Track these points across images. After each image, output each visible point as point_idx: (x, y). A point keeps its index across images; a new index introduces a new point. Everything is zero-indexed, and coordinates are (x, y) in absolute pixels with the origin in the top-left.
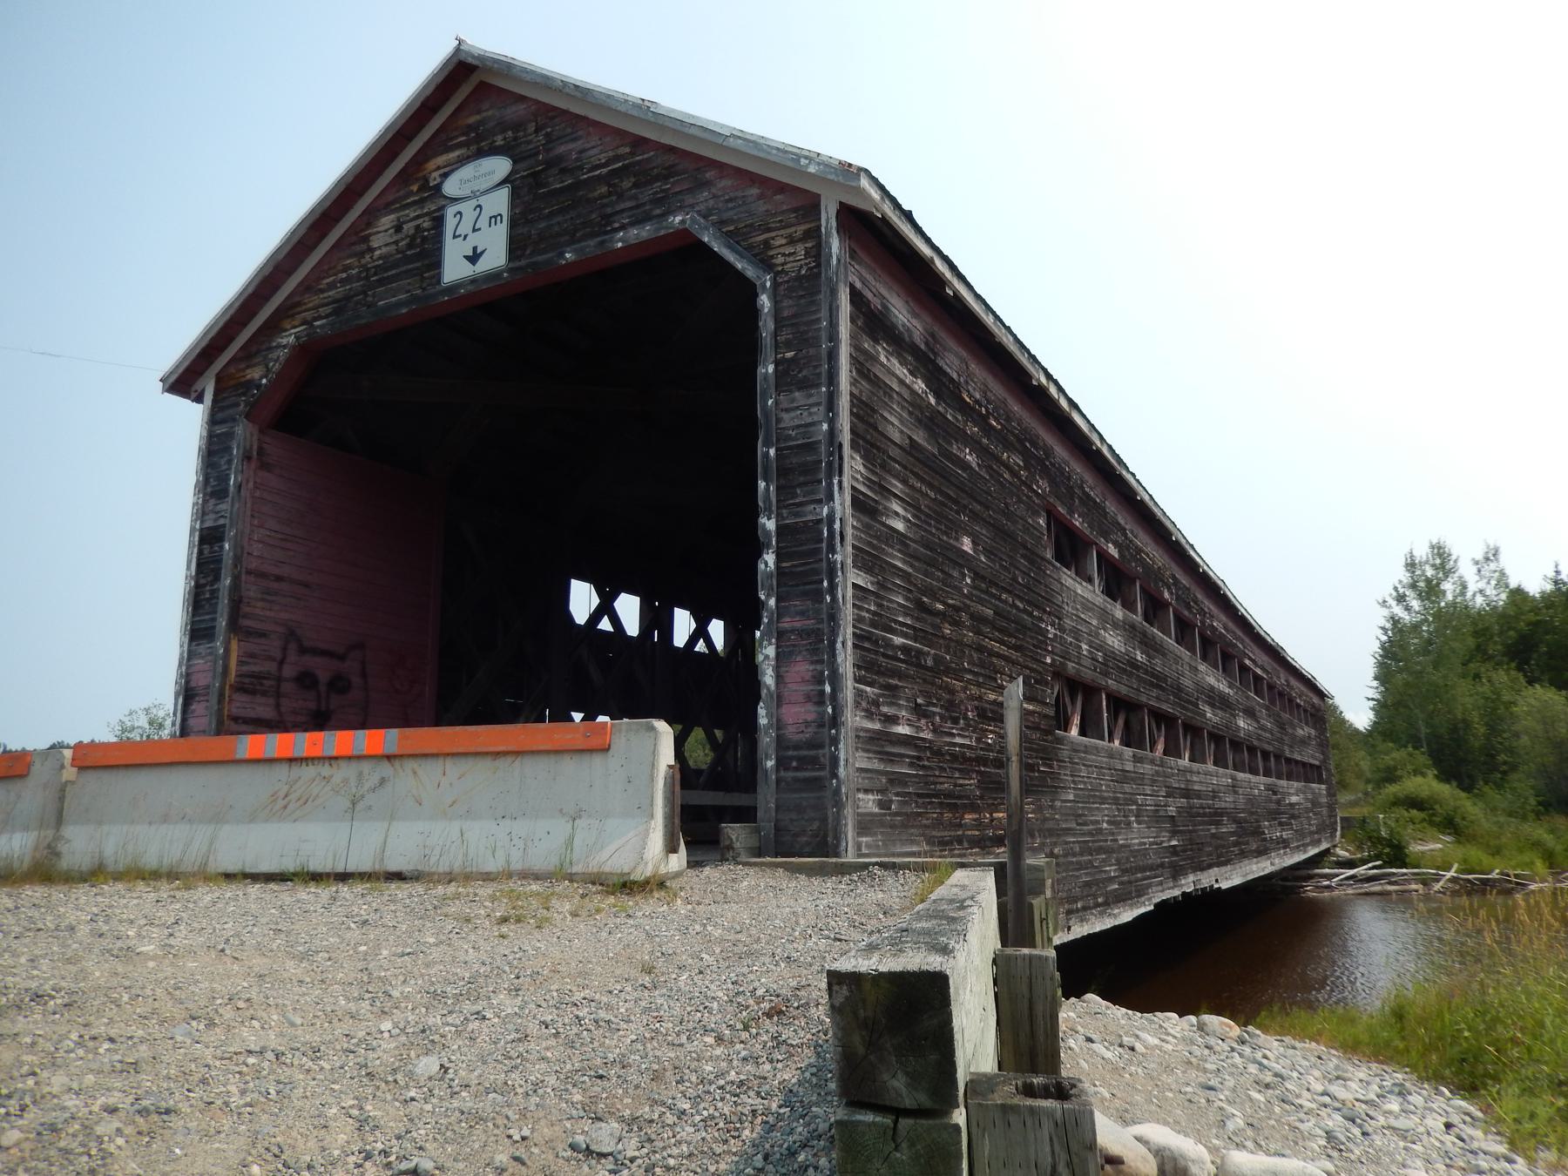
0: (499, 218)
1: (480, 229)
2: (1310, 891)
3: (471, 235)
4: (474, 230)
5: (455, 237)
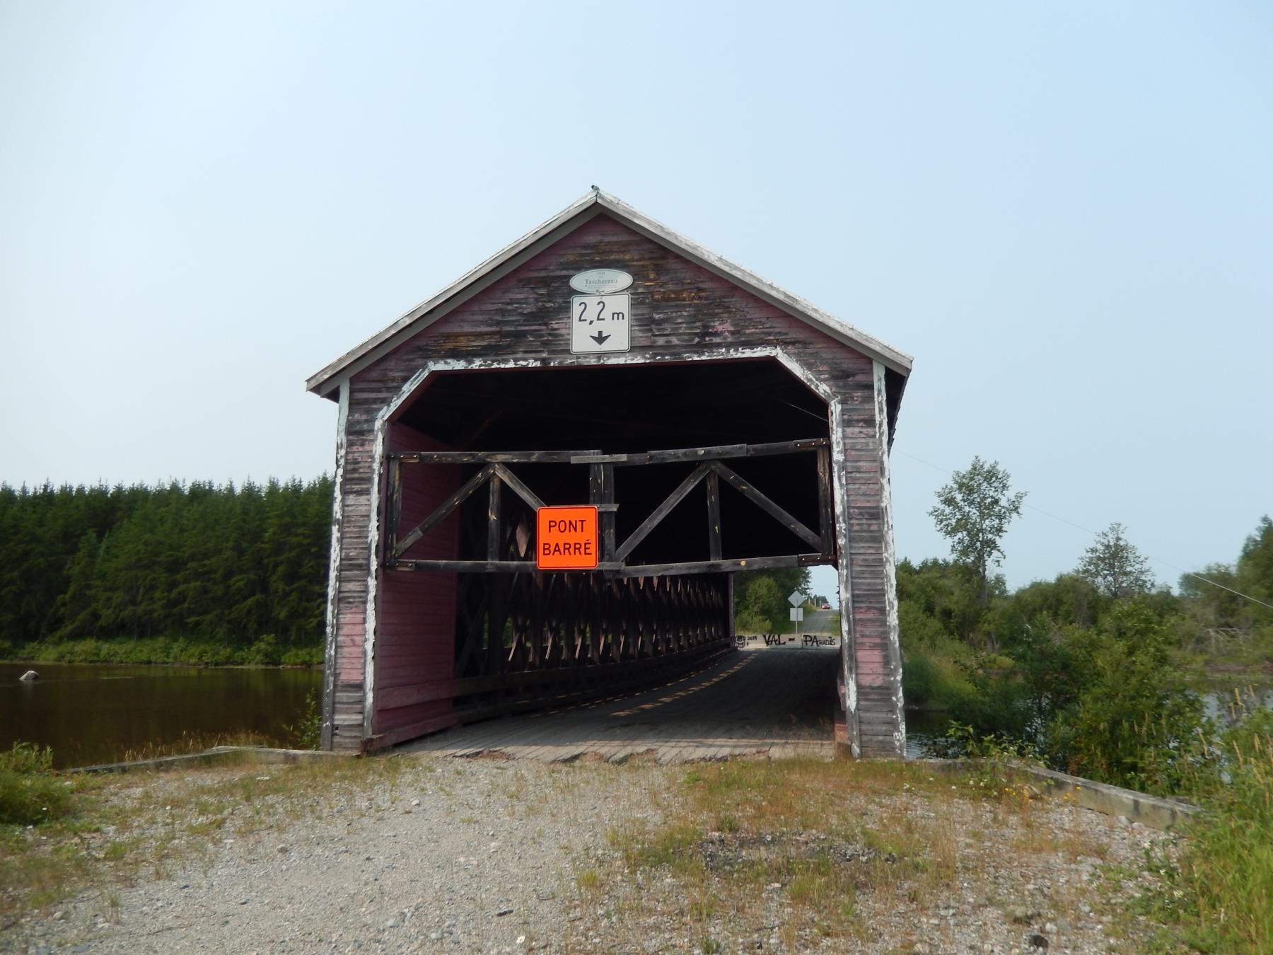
0: (621, 315)
1: (604, 319)
3: (596, 323)
4: (598, 319)
5: (580, 320)
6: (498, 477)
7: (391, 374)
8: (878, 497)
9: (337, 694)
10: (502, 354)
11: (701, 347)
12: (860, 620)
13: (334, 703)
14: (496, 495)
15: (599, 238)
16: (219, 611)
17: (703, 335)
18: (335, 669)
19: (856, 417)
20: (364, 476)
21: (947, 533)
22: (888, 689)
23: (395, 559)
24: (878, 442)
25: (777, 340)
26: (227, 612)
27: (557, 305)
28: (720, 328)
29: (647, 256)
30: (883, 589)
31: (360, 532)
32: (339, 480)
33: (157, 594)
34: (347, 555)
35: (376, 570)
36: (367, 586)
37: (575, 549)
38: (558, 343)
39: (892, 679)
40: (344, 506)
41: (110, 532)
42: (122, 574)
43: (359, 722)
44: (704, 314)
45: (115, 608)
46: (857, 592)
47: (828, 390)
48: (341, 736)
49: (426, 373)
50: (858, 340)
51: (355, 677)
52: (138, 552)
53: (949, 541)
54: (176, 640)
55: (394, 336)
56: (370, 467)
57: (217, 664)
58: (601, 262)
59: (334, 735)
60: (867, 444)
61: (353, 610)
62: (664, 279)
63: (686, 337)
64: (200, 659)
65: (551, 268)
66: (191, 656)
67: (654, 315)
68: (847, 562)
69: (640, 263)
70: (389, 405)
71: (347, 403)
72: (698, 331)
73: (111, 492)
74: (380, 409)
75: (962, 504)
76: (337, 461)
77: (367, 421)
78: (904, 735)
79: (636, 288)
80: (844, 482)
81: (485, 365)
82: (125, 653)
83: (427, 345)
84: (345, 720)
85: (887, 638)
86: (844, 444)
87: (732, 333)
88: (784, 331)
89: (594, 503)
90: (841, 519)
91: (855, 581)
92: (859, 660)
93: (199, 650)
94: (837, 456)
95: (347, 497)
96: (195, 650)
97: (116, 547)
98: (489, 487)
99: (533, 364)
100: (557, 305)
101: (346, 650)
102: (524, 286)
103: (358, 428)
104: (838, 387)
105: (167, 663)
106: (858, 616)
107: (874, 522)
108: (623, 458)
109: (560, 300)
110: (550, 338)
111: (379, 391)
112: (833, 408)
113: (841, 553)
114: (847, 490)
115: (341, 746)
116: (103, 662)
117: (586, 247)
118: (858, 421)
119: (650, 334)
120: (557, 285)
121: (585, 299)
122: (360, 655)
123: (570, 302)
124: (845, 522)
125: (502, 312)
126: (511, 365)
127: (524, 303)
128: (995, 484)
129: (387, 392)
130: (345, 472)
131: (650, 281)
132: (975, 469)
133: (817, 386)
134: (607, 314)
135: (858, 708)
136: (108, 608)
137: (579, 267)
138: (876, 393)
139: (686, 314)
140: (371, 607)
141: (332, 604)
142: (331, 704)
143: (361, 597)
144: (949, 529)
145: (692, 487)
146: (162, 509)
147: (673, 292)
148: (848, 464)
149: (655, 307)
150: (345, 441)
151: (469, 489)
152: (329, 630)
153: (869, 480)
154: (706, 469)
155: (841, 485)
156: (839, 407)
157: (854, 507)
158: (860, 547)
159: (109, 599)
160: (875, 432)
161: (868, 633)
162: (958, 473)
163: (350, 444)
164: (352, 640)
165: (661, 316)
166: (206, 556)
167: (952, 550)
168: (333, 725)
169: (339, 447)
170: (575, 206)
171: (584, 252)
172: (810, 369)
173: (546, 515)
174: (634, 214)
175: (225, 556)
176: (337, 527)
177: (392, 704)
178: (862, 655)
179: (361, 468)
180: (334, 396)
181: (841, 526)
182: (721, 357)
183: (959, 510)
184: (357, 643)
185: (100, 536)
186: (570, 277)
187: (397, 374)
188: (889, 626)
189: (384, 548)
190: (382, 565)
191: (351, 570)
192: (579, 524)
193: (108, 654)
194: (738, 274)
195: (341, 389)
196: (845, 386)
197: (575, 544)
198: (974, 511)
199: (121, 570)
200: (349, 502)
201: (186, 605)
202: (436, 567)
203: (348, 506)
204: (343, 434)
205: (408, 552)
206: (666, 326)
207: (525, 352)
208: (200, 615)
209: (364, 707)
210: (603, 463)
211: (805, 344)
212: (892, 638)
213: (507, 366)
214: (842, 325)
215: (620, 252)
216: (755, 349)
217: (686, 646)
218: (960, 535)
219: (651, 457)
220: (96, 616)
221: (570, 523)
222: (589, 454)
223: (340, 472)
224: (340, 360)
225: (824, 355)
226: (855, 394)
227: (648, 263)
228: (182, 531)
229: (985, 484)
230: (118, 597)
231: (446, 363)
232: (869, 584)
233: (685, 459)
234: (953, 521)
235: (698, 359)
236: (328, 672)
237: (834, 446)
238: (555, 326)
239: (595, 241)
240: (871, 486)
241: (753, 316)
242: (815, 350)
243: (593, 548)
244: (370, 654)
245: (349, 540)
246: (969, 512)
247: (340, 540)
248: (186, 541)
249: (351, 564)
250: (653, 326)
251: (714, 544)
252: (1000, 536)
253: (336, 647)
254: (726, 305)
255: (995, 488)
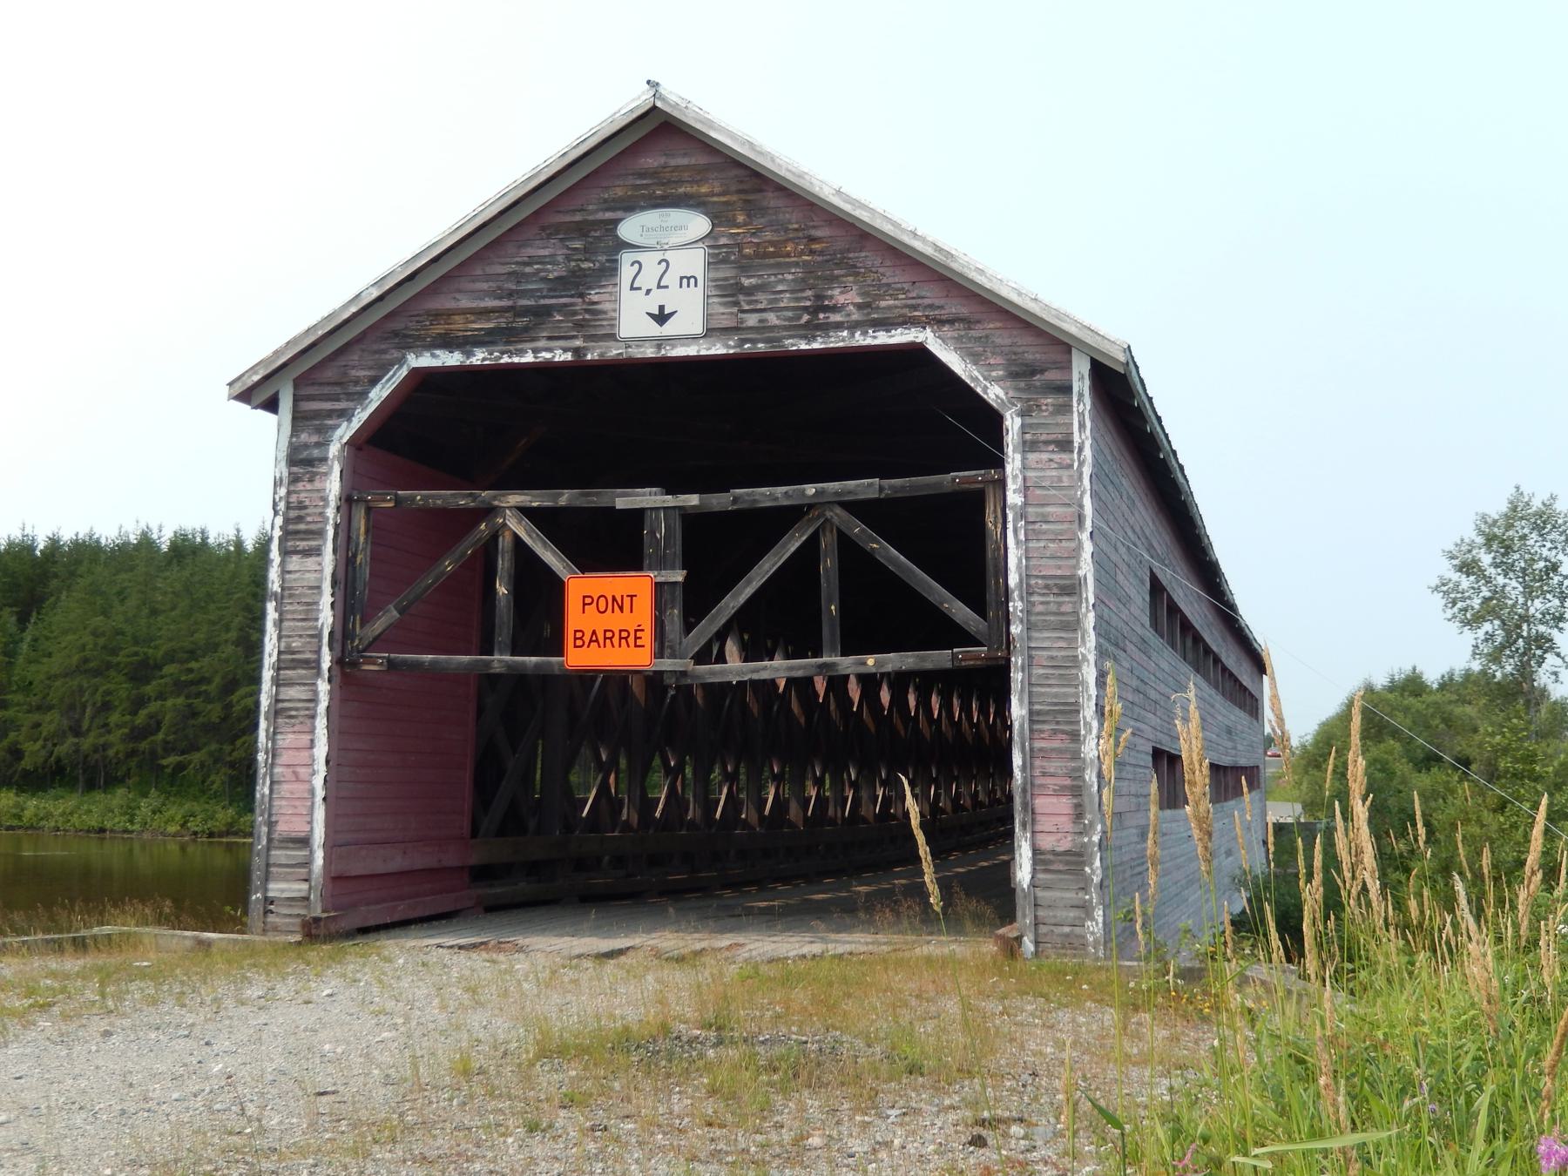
0: (692, 281)
1: (667, 287)
2: (775, 783)
3: (655, 292)
4: (659, 287)
5: (632, 288)
6: (510, 529)
7: (354, 373)
8: (1073, 562)
9: (273, 853)
10: (516, 342)
11: (811, 330)
12: (1041, 750)
13: (268, 865)
14: (507, 557)
15: (662, 160)
16: (214, 746)
17: (815, 311)
18: (270, 815)
19: (1044, 437)
20: (313, 527)
21: (1466, 623)
22: (1080, 854)
23: (359, 652)
24: (1076, 474)
25: (927, 317)
26: (227, 748)
27: (597, 264)
28: (841, 299)
29: (733, 188)
30: (1076, 703)
31: (307, 611)
32: (277, 533)
33: (114, 718)
34: (288, 646)
35: (330, 670)
36: (316, 693)
37: (621, 638)
38: (594, 323)
39: (1086, 840)
40: (284, 572)
41: (38, 613)
42: (58, 683)
43: (303, 894)
44: (818, 278)
45: (46, 740)
46: (1037, 707)
47: (1001, 394)
48: (278, 914)
49: (404, 372)
50: (1044, 316)
51: (299, 828)
52: (83, 647)
53: (1469, 638)
54: (145, 795)
55: (355, 315)
56: (322, 514)
57: (211, 835)
58: (663, 197)
59: (267, 912)
60: (1060, 479)
61: (296, 729)
62: (759, 222)
63: (790, 314)
64: (182, 826)
65: (590, 207)
66: (171, 820)
67: (743, 280)
68: (1023, 660)
69: (723, 199)
70: (349, 420)
71: (289, 417)
72: (808, 303)
73: (41, 546)
74: (337, 427)
75: (1491, 571)
76: (275, 504)
77: (318, 445)
78: (1101, 925)
79: (716, 239)
80: (1022, 537)
81: (490, 359)
82: (63, 814)
83: (406, 328)
84: (283, 891)
85: (1081, 778)
86: (1025, 479)
87: (859, 306)
88: (937, 302)
89: (650, 569)
90: (1016, 594)
91: (1035, 689)
92: (1038, 810)
93: (182, 812)
94: (1014, 498)
95: (288, 559)
96: (175, 811)
97: (47, 638)
98: (497, 545)
99: (562, 357)
100: (597, 264)
101: (285, 787)
102: (549, 237)
103: (304, 455)
104: (1018, 389)
105: (132, 832)
106: (1038, 744)
107: (1067, 599)
108: (693, 500)
109: (603, 258)
110: (587, 316)
111: (335, 398)
112: (1008, 423)
113: (1015, 647)
114: (1027, 550)
115: (276, 929)
116: (27, 828)
117: (642, 175)
118: (1047, 443)
119: (735, 310)
120: (598, 234)
121: (641, 257)
122: (306, 795)
123: (617, 261)
124: (1021, 599)
125: (516, 276)
126: (529, 358)
127: (549, 263)
128: (1554, 536)
129: (347, 401)
130: (287, 521)
131: (738, 227)
132: (1514, 509)
133: (985, 389)
134: (671, 279)
135: (1033, 885)
136: (35, 741)
137: (631, 206)
138: (1075, 399)
139: (790, 277)
140: (321, 723)
141: (266, 719)
142: (263, 867)
143: (307, 709)
144: (1469, 616)
145: (797, 544)
146: (124, 576)
147: (772, 243)
148: (1030, 509)
149: (744, 267)
150: (285, 474)
151: (467, 548)
152: (261, 757)
153: (1061, 534)
154: (819, 517)
155: (1018, 542)
156: (1018, 421)
157: (1037, 577)
158: (1043, 638)
159: (37, 725)
160: (1073, 460)
161: (1052, 770)
162: (1484, 518)
163: (294, 479)
164: (294, 772)
165: (753, 281)
166: (192, 654)
167: (1474, 653)
168: (266, 898)
169: (277, 483)
170: (622, 112)
171: (638, 182)
172: (976, 363)
173: (579, 586)
174: (711, 124)
175: (223, 655)
176: (274, 603)
177: (358, 868)
178: (1041, 803)
179: (308, 515)
180: (271, 405)
181: (1016, 605)
182: (841, 344)
183: (1487, 582)
184: (302, 776)
185: (23, 620)
186: (616, 222)
187: (362, 373)
188: (1084, 759)
189: (343, 636)
190: (339, 662)
191: (294, 668)
192: (627, 601)
193: (36, 815)
194: (864, 216)
195: (281, 396)
196: (1029, 388)
197: (621, 631)
198: (1514, 583)
199: (56, 677)
200: (291, 567)
201: (160, 736)
202: (419, 664)
203: (289, 572)
204: (283, 464)
205: (377, 643)
206: (761, 296)
207: (550, 338)
208: (183, 753)
209: (310, 872)
210: (664, 508)
211: (968, 322)
212: (1087, 777)
213: (523, 360)
214: (1020, 294)
215: (693, 182)
216: (893, 331)
217: (949, 808)
218: (1487, 627)
219: (736, 500)
220: (16, 753)
221: (614, 598)
222: (644, 495)
223: (279, 521)
224: (277, 353)
225: (999, 341)
226: (1042, 401)
227: (734, 198)
228: (154, 612)
229: (1534, 536)
230: (52, 721)
231: (433, 356)
232: (1056, 695)
233: (786, 503)
234: (1476, 603)
235: (807, 347)
236: (260, 819)
237: (1009, 481)
238: (595, 298)
239: (656, 164)
240: (1064, 544)
241: (890, 280)
242: (983, 333)
243: (647, 638)
244: (320, 793)
245: (292, 624)
246: (1504, 586)
247: (279, 623)
248: (160, 629)
249: (293, 660)
250: (741, 297)
251: (830, 630)
252: (1561, 629)
253: (272, 783)
254: (851, 262)
255: (1552, 541)
